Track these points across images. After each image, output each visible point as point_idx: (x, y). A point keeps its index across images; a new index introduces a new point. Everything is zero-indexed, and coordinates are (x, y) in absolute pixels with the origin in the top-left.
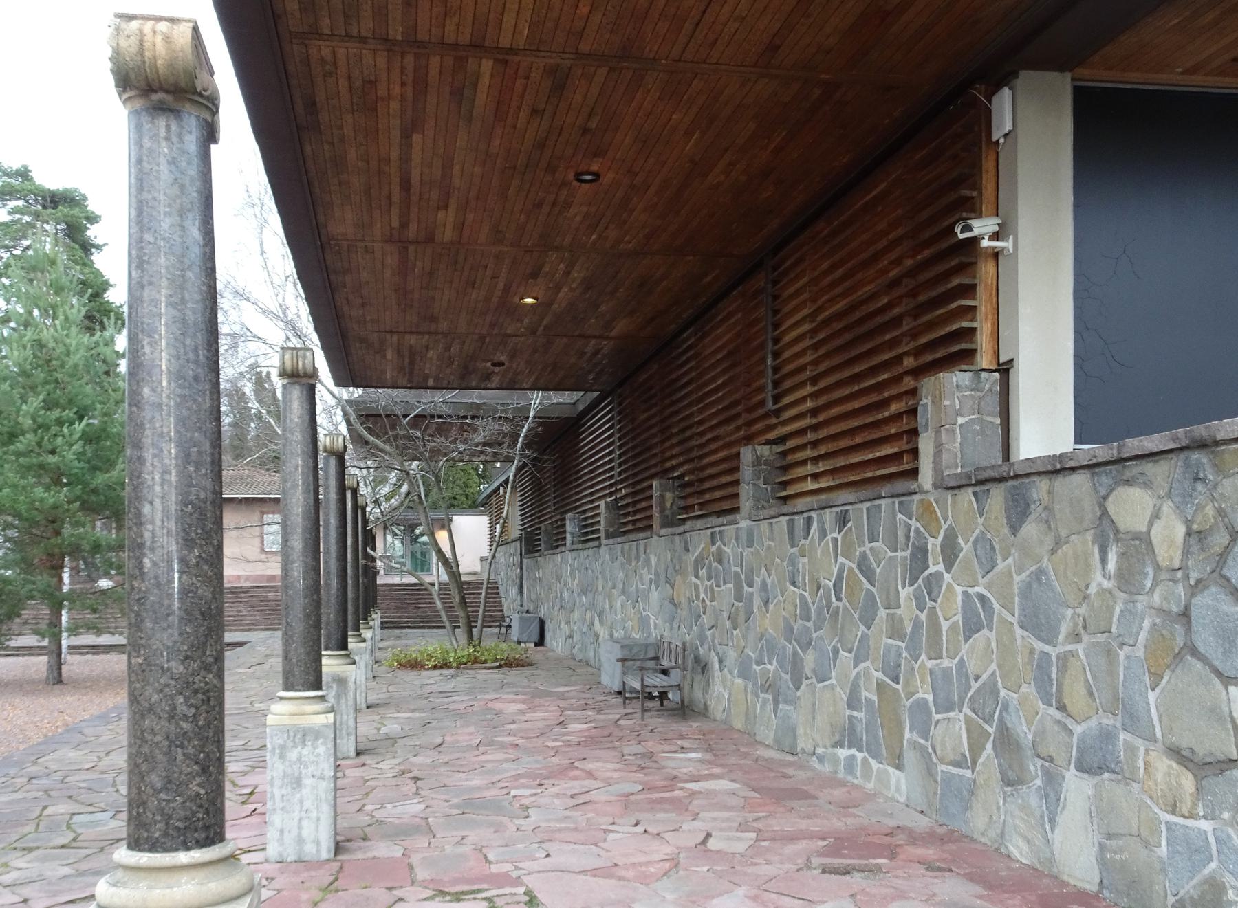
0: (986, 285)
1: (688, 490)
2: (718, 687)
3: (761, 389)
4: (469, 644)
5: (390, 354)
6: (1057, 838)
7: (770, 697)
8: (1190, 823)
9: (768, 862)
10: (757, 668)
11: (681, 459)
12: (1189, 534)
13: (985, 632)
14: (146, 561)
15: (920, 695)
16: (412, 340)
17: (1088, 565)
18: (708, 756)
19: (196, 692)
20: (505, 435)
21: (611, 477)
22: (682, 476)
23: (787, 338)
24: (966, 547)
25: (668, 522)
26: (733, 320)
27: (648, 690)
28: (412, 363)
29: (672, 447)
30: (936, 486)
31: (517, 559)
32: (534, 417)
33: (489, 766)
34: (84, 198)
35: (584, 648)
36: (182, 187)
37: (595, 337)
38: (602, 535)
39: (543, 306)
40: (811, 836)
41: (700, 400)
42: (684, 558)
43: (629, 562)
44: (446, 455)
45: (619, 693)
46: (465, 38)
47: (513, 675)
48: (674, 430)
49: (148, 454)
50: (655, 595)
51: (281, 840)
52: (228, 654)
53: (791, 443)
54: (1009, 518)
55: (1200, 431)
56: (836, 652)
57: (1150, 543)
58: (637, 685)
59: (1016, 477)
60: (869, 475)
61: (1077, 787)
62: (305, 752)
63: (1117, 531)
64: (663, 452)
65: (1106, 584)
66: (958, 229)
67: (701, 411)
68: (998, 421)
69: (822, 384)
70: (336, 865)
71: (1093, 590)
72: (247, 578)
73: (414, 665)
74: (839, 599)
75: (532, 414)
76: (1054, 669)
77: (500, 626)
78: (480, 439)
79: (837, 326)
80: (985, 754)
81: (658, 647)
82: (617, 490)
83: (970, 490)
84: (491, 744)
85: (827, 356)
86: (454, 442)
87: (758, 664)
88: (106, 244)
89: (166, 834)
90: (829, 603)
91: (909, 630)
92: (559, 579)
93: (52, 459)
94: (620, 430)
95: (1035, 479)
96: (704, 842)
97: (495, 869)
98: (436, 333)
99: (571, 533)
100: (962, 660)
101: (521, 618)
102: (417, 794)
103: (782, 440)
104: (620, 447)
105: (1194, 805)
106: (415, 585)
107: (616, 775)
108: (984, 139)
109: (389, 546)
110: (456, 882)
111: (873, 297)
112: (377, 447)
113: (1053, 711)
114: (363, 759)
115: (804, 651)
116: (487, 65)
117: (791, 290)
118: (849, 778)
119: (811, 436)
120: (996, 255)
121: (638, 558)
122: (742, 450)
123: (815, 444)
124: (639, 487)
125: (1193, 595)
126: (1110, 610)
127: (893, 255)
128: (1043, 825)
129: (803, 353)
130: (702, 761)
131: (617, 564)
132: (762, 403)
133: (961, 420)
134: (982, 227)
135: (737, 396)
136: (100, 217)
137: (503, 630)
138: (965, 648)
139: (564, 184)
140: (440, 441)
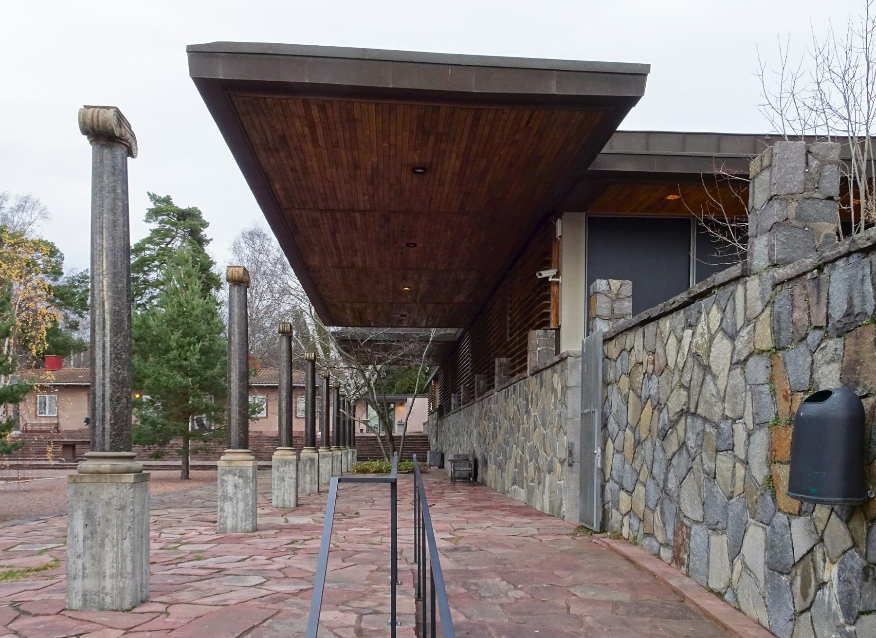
5: (348, 311)
16: (357, 305)
32: (432, 341)
34: (200, 212)
49: (232, 362)
51: (277, 500)
62: (286, 468)
66: (537, 275)
88: (211, 239)
93: (185, 363)
133: (539, 349)
136: (208, 223)
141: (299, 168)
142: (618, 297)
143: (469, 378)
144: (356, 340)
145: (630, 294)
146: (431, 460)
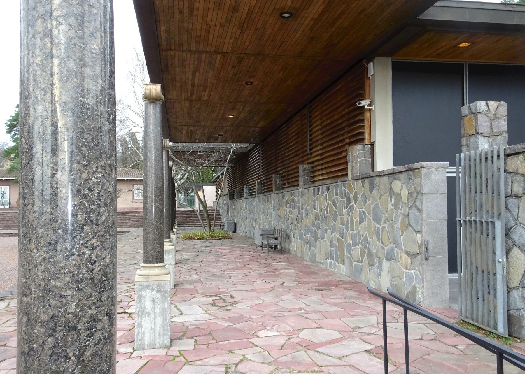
0: (367, 119)
1: (284, 178)
2: (293, 243)
3: (306, 146)
4: (210, 231)
5: (184, 132)
6: (381, 280)
7: (308, 245)
8: (410, 271)
9: (300, 288)
10: (305, 236)
11: (282, 168)
12: (409, 193)
13: (364, 222)
14: (148, 200)
15: (349, 242)
16: (192, 128)
17: (388, 202)
18: (288, 264)
19: (159, 229)
20: (223, 158)
21: (259, 173)
22: (282, 173)
23: (314, 130)
24: (360, 197)
25: (278, 189)
26: (297, 123)
27: (270, 244)
28: (191, 135)
29: (279, 163)
30: (352, 179)
31: (226, 201)
32: (233, 152)
33: (219, 266)
35: (250, 232)
36: (157, 119)
37: (253, 127)
38: (256, 193)
39: (235, 118)
40: (314, 282)
41: (288, 148)
42: (283, 201)
43: (265, 202)
44: (202, 165)
45: (261, 246)
46: (213, 50)
47: (225, 241)
48: (280, 158)
50: (273, 214)
52: (119, 236)
53: (315, 164)
54: (370, 189)
55: (410, 166)
56: (327, 230)
57: (401, 196)
58: (266, 243)
59: (371, 177)
60: (336, 175)
61: (386, 264)
63: (394, 193)
64: (276, 165)
65: (392, 207)
66: (357, 103)
67: (288, 152)
68: (370, 160)
69: (324, 145)
70: (175, 290)
71: (389, 209)
72: (128, 209)
73: (191, 238)
74: (327, 213)
75: (232, 151)
76: (381, 232)
77: (220, 226)
78: (214, 159)
79: (328, 128)
80: (365, 258)
81: (274, 230)
82: (261, 178)
83: (360, 180)
84: (219, 261)
85: (325, 137)
86: (205, 160)
87: (305, 235)
89: (152, 260)
90: (325, 215)
91: (346, 222)
92: (241, 209)
94: (262, 157)
95: (376, 178)
96: (282, 284)
97: (221, 290)
98: (200, 126)
99: (246, 192)
100: (359, 230)
101: (228, 223)
102: (196, 273)
103: (312, 163)
104: (262, 163)
105: (410, 267)
106: (192, 211)
107: (258, 269)
108: (366, 76)
109: (180, 197)
110: (211, 293)
111: (337, 120)
112: (178, 163)
113: (380, 244)
114: (178, 265)
115: (318, 230)
116: (219, 56)
117: (315, 115)
118: (330, 269)
119: (321, 162)
120: (370, 110)
121: (268, 201)
122: (300, 166)
123: (322, 164)
124: (268, 177)
125: (410, 210)
126: (392, 214)
127: (342, 108)
128: (378, 277)
129: (318, 135)
130: (286, 265)
131: (261, 203)
132: (306, 151)
133: (359, 160)
134: (365, 103)
135: (299, 148)
137: (221, 227)
138: (360, 227)
139: (242, 85)
140: (200, 161)
141: (186, 10)
142: (495, 117)
143: (259, 176)
144: (184, 151)
145: (506, 114)
146: (228, 228)
